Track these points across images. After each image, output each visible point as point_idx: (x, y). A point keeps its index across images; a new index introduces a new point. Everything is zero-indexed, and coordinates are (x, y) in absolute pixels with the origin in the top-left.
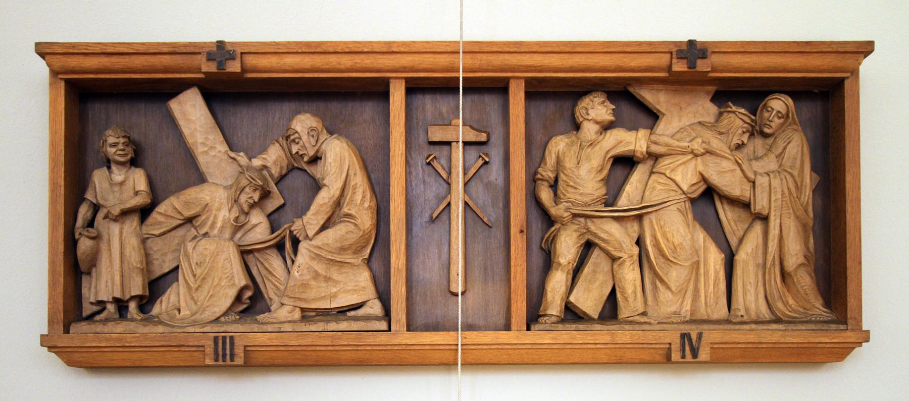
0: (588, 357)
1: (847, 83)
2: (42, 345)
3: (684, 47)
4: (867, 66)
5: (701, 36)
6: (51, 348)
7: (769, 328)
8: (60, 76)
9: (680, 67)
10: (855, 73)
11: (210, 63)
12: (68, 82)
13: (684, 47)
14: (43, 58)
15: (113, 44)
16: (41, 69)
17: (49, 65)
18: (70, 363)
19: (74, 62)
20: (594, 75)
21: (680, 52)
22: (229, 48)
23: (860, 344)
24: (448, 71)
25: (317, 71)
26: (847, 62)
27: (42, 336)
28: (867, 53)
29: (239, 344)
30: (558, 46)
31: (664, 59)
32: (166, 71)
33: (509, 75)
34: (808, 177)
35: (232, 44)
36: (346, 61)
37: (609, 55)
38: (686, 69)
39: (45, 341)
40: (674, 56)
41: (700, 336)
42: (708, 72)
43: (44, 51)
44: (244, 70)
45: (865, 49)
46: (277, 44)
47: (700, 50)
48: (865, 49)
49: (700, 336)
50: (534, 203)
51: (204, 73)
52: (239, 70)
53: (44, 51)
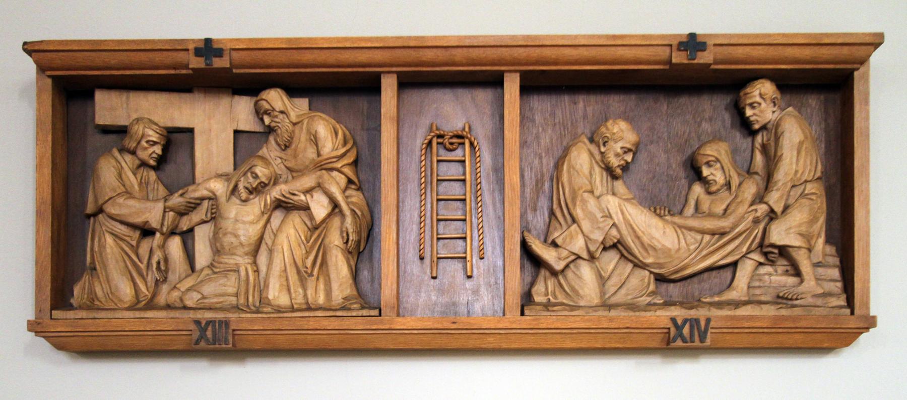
0: (744, 341)
1: (856, 73)
2: (30, 330)
3: (202, 45)
4: (877, 58)
5: (700, 29)
6: (37, 333)
7: (146, 316)
8: (49, 73)
9: (679, 58)
10: (863, 61)
11: (683, 54)
12: (54, 78)
13: (202, 45)
14: (30, 56)
15: (339, 40)
16: (29, 66)
17: (36, 62)
18: (60, 346)
19: (58, 59)
20: (286, 70)
21: (681, 44)
22: (699, 40)
23: (867, 329)
24: (417, 65)
25: (339, 67)
26: (859, 52)
27: (28, 321)
28: (877, 45)
29: (233, 326)
30: (353, 43)
31: (664, 53)
32: (537, 63)
33: (503, 68)
34: (414, 166)
35: (219, 41)
36: (282, 57)
37: (390, 50)
38: (686, 61)
39: (35, 327)
40: (674, 48)
41: (708, 321)
42: (710, 65)
43: (30, 49)
44: (232, 65)
45: (875, 42)
46: (769, 35)
47: (700, 43)
48: (875, 42)
49: (708, 321)
50: (771, 185)
51: (192, 69)
52: (228, 66)
53: (30, 49)
